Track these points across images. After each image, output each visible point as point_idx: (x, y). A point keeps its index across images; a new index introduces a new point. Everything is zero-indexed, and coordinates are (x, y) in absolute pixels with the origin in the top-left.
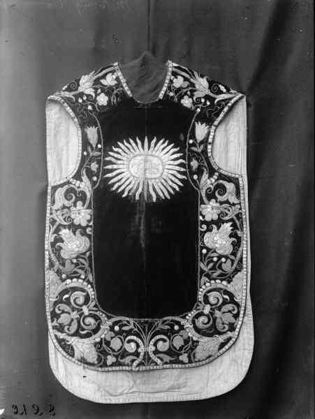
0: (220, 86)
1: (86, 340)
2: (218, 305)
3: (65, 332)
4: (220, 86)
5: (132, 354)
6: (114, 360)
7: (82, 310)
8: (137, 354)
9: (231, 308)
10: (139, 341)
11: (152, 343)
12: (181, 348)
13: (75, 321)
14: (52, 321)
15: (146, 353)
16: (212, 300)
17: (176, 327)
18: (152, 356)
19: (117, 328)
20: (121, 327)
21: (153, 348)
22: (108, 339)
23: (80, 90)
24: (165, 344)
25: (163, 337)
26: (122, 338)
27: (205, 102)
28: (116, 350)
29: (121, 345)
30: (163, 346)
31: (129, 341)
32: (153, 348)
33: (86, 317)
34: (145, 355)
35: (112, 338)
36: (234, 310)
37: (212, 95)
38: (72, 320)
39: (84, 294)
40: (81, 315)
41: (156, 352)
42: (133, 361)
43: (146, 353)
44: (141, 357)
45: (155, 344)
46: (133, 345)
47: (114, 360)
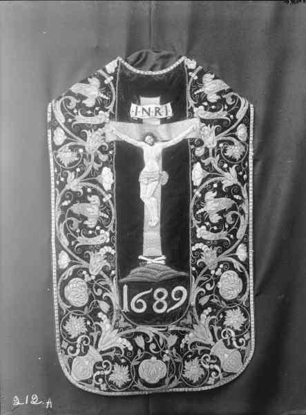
0: (69, 202)
4: (69, 202)
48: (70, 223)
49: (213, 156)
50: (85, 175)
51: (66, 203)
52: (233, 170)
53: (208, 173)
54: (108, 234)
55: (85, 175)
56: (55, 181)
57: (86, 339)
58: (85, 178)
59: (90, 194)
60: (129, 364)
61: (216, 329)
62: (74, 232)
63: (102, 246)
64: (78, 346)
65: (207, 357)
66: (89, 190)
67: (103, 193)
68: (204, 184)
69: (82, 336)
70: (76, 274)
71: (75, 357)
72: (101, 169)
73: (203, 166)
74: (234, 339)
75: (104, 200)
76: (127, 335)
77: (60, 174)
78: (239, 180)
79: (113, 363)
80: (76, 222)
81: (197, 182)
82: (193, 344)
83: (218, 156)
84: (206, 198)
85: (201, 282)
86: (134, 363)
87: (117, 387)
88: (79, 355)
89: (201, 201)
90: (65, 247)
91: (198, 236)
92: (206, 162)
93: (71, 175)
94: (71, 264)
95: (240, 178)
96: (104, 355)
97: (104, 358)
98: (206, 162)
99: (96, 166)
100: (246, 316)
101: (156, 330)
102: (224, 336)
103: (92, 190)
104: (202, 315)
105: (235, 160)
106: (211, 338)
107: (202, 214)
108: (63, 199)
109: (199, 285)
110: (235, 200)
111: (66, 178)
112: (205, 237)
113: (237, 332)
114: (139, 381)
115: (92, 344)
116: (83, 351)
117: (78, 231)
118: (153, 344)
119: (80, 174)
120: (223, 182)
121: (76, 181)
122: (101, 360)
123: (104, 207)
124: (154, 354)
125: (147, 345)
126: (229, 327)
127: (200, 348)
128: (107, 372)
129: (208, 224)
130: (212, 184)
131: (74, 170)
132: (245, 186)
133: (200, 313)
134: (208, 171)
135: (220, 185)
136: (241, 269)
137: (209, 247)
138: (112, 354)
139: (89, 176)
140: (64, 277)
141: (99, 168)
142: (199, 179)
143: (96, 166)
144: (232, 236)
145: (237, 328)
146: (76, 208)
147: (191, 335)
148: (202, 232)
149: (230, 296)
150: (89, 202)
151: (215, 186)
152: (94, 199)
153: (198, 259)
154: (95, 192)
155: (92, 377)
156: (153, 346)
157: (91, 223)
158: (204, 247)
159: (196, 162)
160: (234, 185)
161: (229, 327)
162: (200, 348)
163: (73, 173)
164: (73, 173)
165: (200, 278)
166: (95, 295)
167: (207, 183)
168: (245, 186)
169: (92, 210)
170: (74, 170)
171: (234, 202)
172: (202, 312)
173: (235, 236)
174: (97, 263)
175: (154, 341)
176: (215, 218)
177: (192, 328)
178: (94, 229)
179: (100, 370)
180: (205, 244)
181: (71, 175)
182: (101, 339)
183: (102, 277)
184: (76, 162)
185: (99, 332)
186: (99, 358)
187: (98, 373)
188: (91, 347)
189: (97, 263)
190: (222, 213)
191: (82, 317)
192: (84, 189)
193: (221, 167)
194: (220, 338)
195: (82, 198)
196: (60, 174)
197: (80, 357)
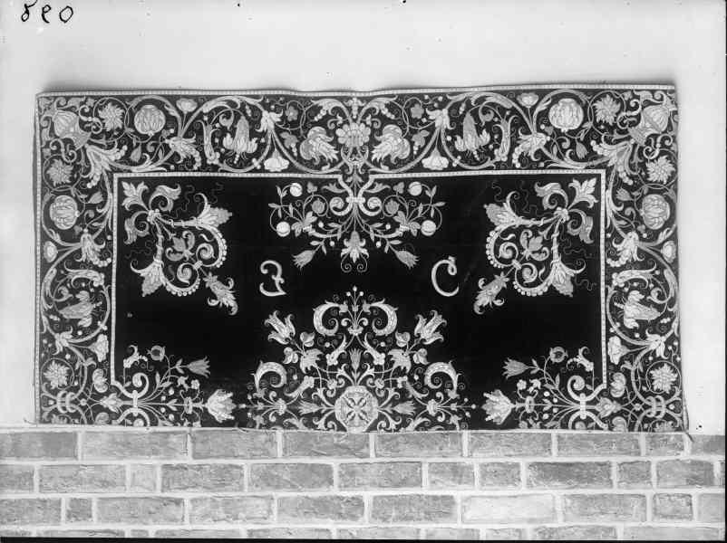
0: (662, 322)
1: (503, 227)
2: (516, 249)
3: (530, 229)
4: (662, 322)
5: (373, 195)
6: (395, 188)
7: (521, 263)
8: (367, 196)
9: (172, 255)
10: (363, 210)
11: (348, 210)
12: (315, 199)
13: (181, 257)
14: (110, 265)
15: (356, 195)
16: (507, 255)
17: (321, 225)
18: (350, 191)
19: (388, 227)
20: (383, 228)
21: (348, 200)
22: (400, 213)
23: (445, 111)
24: (335, 205)
25: (339, 214)
26: (384, 214)
27: (673, 346)
28: (392, 201)
29: (387, 206)
30: (336, 203)
31: (377, 208)
32: (348, 200)
33: (513, 258)
34: (357, 193)
35: (396, 215)
36: (170, 252)
37: (669, 334)
38: (181, 253)
39: (674, 169)
40: (520, 256)
41: (344, 196)
42: (372, 187)
43: (356, 195)
44: (361, 191)
45: (346, 204)
46: (372, 206)
47: (395, 188)
48: (661, 297)
49: (83, 367)
50: (642, 354)
51: (665, 321)
52: (59, 349)
53: (89, 347)
54: (615, 283)
55: (642, 354)
56: (40, 353)
57: (648, 153)
58: (641, 351)
59: (635, 330)
60: (595, 122)
61: (82, 162)
62: (656, 285)
63: (623, 268)
64: (658, 145)
65: (94, 130)
66: (637, 335)
67: (620, 333)
68: (93, 335)
69: (652, 158)
70: (655, 234)
71: (663, 133)
72: (622, 360)
73: (95, 357)
74: (63, 150)
75: (618, 324)
76: (596, 158)
77: (674, 355)
78: (53, 336)
79: (615, 125)
80: (654, 297)
81: (102, 338)
82: (110, 147)
83: (77, 368)
84: (90, 319)
85: (101, 221)
86: (589, 125)
87: (612, 96)
88: (80, 120)
89: (97, 315)
90: (669, 269)
91: (103, 276)
92: (90, 362)
93: (660, 352)
94: (661, 246)
95: (52, 340)
96: (626, 136)
97: (626, 132)
98: (90, 362)
99: (627, 365)
100: (47, 176)
101: (562, 164)
102: (73, 154)
103: (633, 335)
104: (98, 179)
105: (57, 362)
106: (88, 151)
107: (97, 301)
108: (669, 325)
109: (103, 218)
110: (58, 315)
111: (667, 350)
112: (94, 273)
113: (60, 158)
114: (584, 102)
115: (93, 136)
116: (87, 125)
117: (651, 285)
118: (566, 148)
119: (646, 356)
120: (71, 336)
121: (652, 347)
122: (630, 130)
123: (617, 315)
124: (565, 136)
125: (573, 146)
126: (68, 164)
127: (102, 141)
128: (624, 114)
129: (92, 290)
130: (84, 335)
131: (655, 359)
132: (45, 330)
133: (101, 183)
134: (89, 351)
135: (75, 335)
136: (52, 233)
137: (91, 262)
138: (616, 136)
139: (637, 354)
140: (668, 231)
141: (660, 357)
142: (101, 343)
143: (627, 365)
144: (62, 272)
145: (58, 163)
146: (651, 314)
147: (113, 158)
148: (98, 280)
149: (64, 199)
150: (637, 321)
151: (80, 333)
152: (630, 324)
153: (105, 249)
154: (631, 333)
155: (643, 109)
156: (566, 145)
157: (635, 296)
158: (97, 262)
159: (103, 362)
160: (60, 332)
161: (68, 164)
162: (102, 141)
163: (658, 355)
164: (658, 355)
165: (103, 225)
166: (633, 207)
167: (89, 338)
168: (45, 330)
169: (633, 312)
170: (655, 359)
171: (61, 312)
172: (99, 182)
173: (58, 272)
174: (630, 246)
175: (564, 151)
176: (83, 295)
177: (612, 167)
178: (632, 289)
179: (631, 116)
180: (97, 266)
181: (660, 352)
182: (98, 148)
183: (623, 229)
184: (652, 369)
185: (632, 163)
186: (632, 131)
187: (635, 113)
188: (90, 133)
189: (630, 246)
190: (75, 301)
191: (651, 182)
192: (644, 337)
193: (72, 354)
194: (78, 152)
195: (645, 327)
196: (674, 355)
197: (656, 132)
